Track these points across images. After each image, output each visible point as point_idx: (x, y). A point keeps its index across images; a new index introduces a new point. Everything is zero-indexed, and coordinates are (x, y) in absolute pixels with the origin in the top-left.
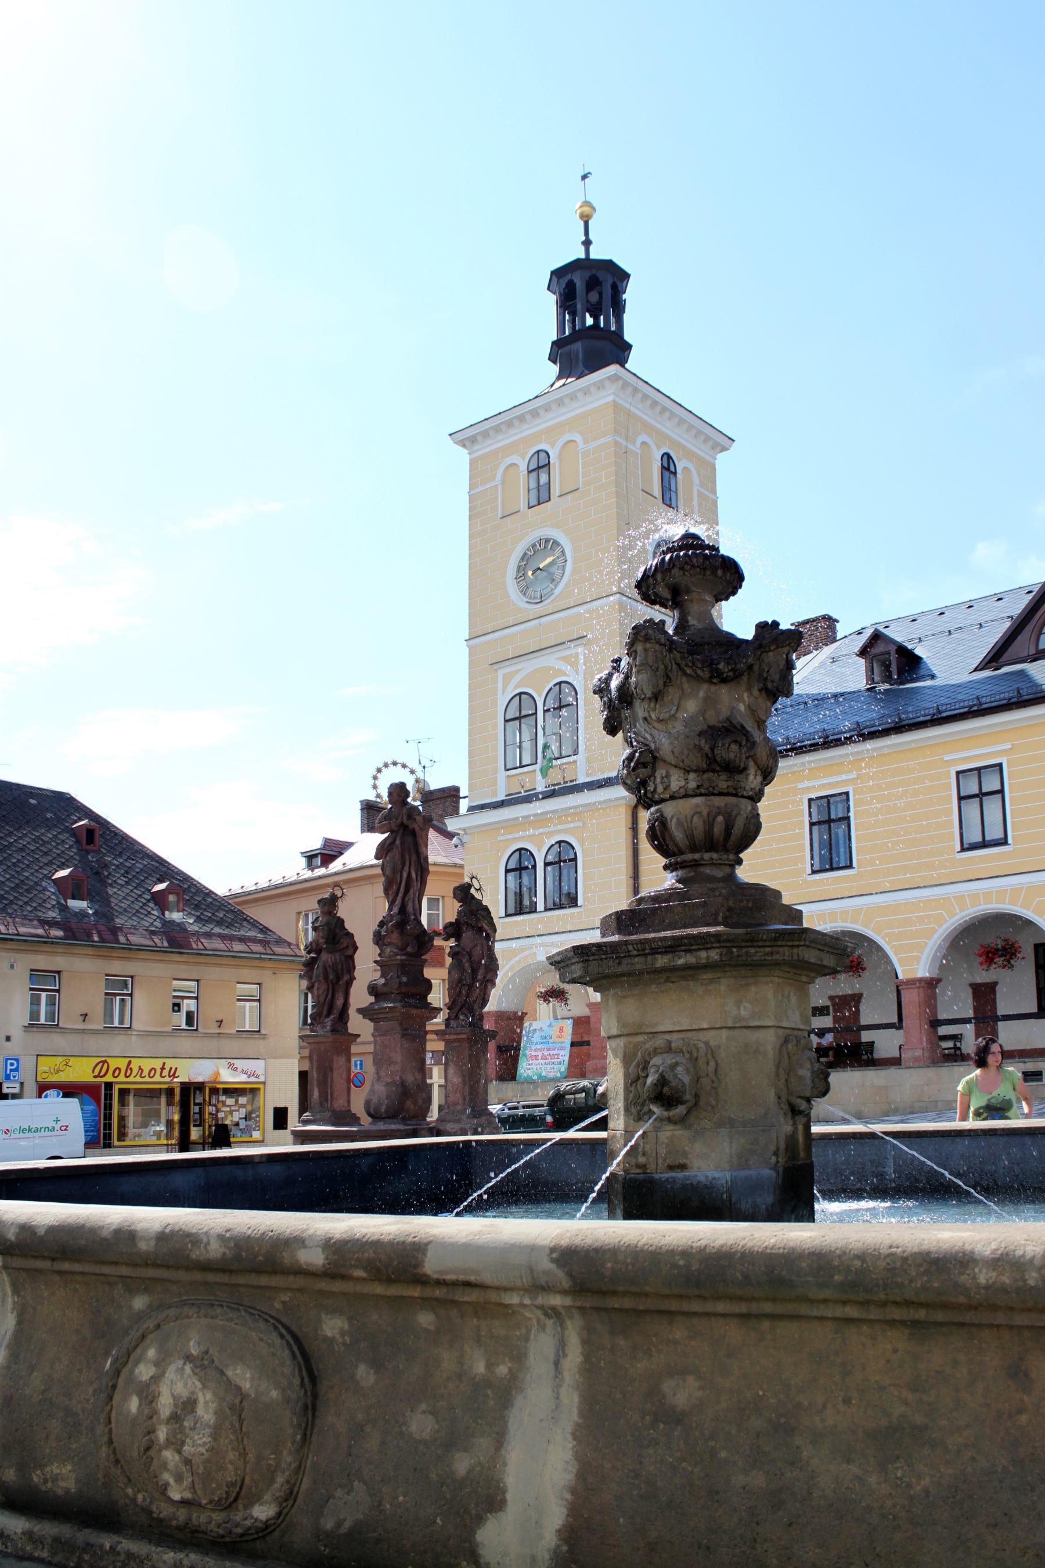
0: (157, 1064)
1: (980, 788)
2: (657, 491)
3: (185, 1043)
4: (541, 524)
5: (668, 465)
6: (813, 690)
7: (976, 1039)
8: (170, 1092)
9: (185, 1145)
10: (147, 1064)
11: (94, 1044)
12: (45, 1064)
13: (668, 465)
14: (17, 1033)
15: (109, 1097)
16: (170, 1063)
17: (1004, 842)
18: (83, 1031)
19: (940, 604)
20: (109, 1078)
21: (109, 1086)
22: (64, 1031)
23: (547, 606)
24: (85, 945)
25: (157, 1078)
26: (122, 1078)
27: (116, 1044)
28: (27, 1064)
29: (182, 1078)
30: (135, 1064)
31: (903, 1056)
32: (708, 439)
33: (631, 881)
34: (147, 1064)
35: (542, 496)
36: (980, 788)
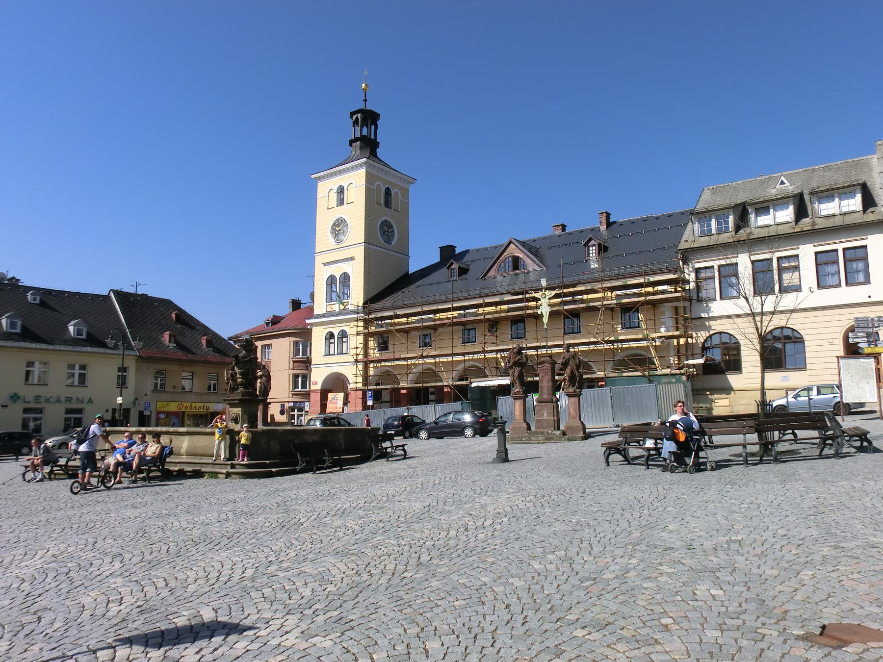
2: (383, 202)
3: (213, 397)
5: (388, 192)
6: (62, 482)
8: (207, 415)
9: (713, 278)
12: (159, 404)
13: (388, 192)
14: (149, 393)
16: (207, 405)
19: (496, 244)
20: (183, 410)
21: (184, 413)
22: (167, 392)
24: (348, 169)
28: (153, 404)
29: (211, 410)
31: (760, 375)
32: (405, 180)
34: (198, 405)
35: (341, 202)
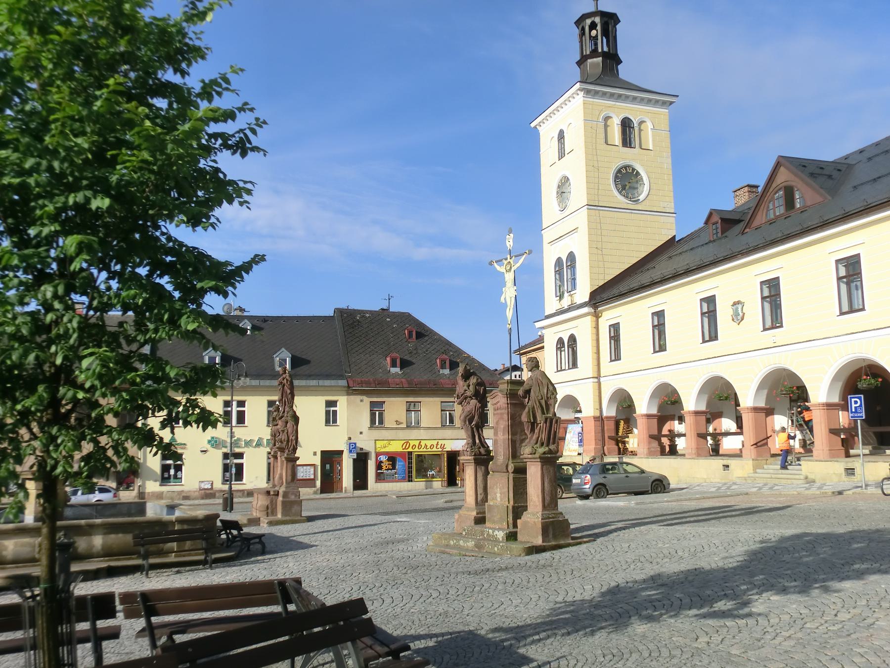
0: (435, 442)
1: (851, 271)
4: (629, 157)
7: (222, 521)
10: (429, 443)
11: (402, 434)
12: (379, 444)
15: (410, 458)
16: (441, 442)
17: (863, 309)
18: (396, 429)
20: (410, 450)
21: (410, 453)
23: (567, 212)
25: (435, 449)
26: (416, 449)
27: (414, 434)
30: (423, 443)
33: (595, 355)
34: (429, 443)
36: (851, 271)
